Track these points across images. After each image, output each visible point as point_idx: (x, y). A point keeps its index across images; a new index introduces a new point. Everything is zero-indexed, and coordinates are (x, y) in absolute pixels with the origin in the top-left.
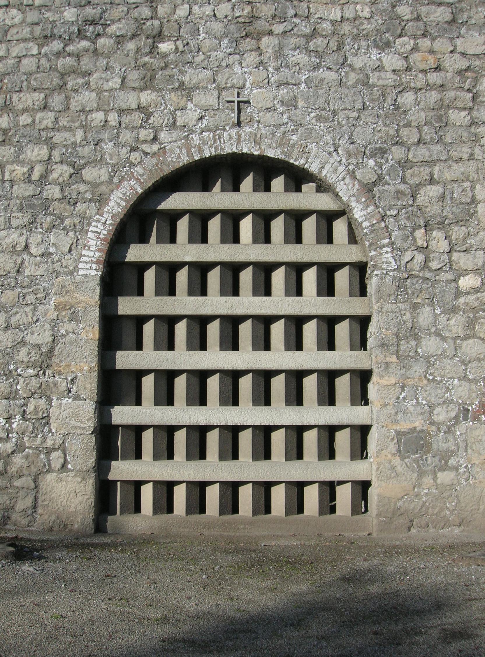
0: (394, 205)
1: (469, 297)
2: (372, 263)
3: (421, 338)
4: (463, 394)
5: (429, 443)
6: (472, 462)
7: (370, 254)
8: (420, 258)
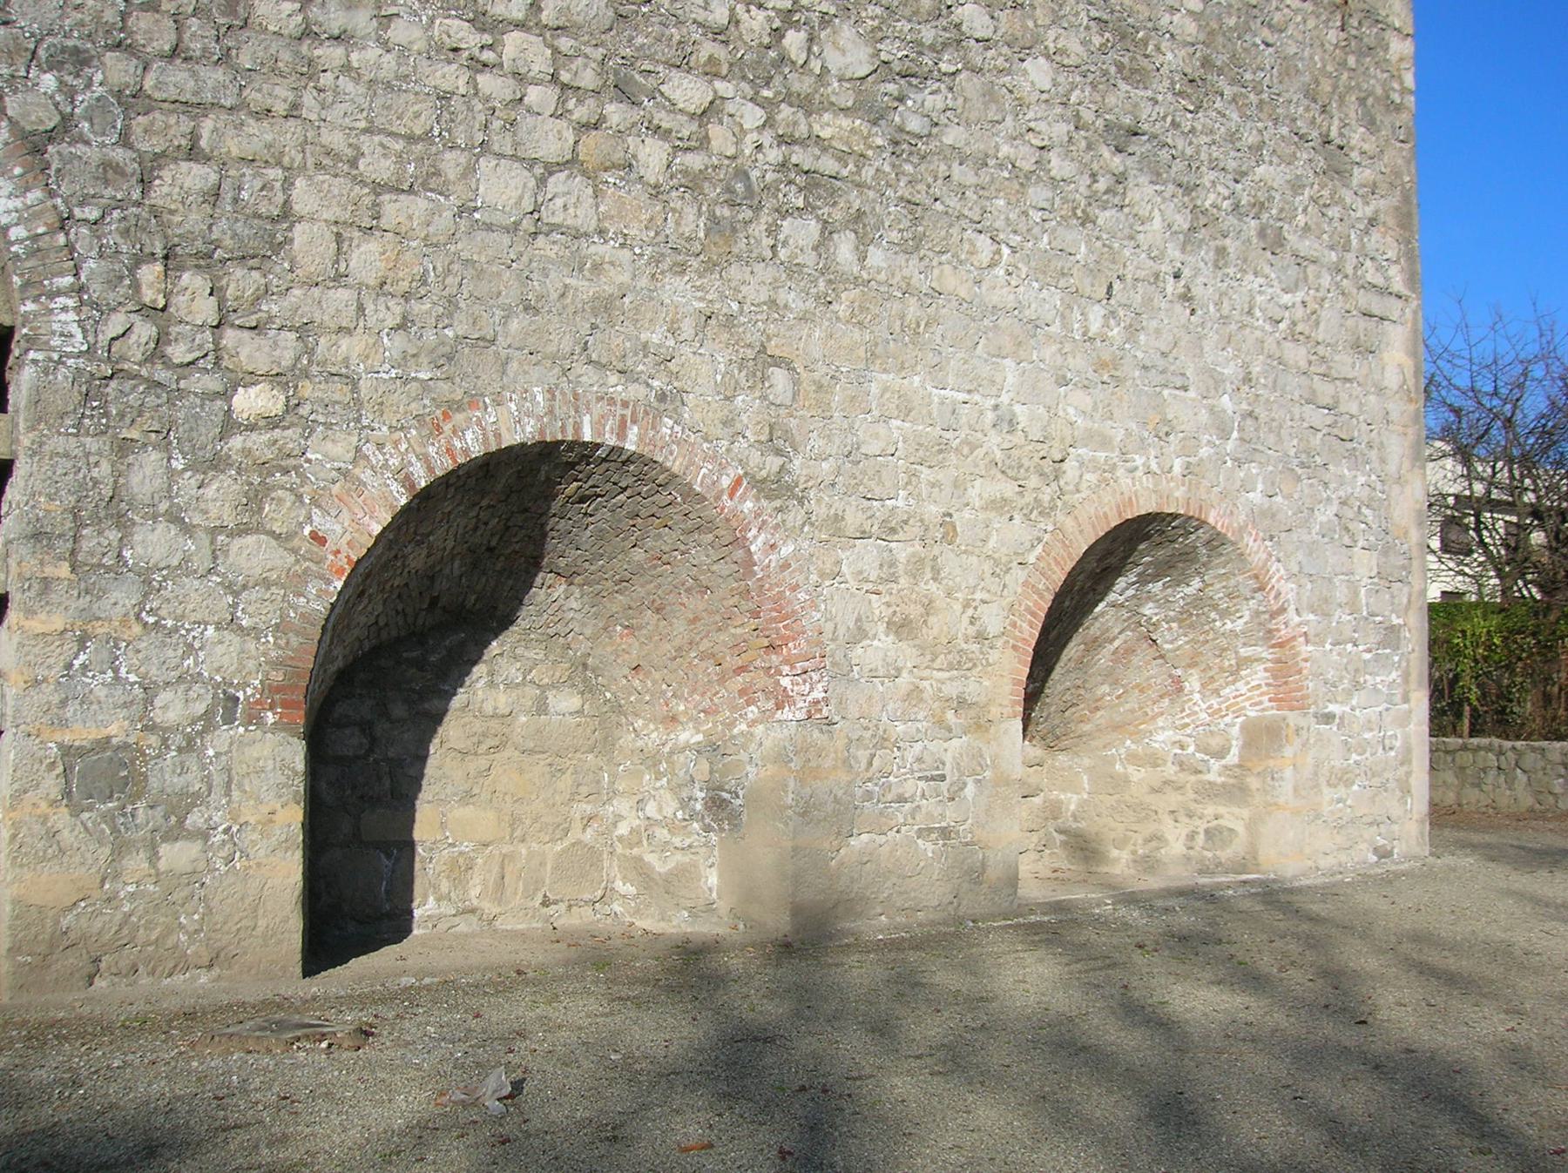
0: (93, 197)
1: (254, 436)
2: (25, 331)
3: (134, 524)
4: (226, 661)
5: (141, 774)
6: (242, 821)
7: (23, 308)
8: (144, 331)
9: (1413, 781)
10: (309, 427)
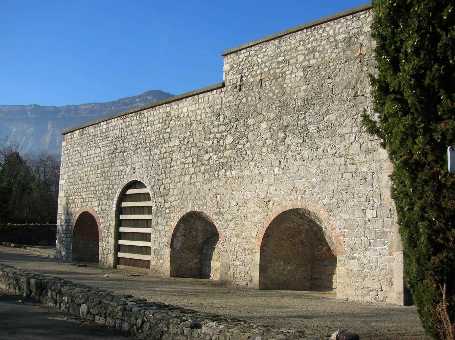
9: (394, 280)
10: (171, 213)
